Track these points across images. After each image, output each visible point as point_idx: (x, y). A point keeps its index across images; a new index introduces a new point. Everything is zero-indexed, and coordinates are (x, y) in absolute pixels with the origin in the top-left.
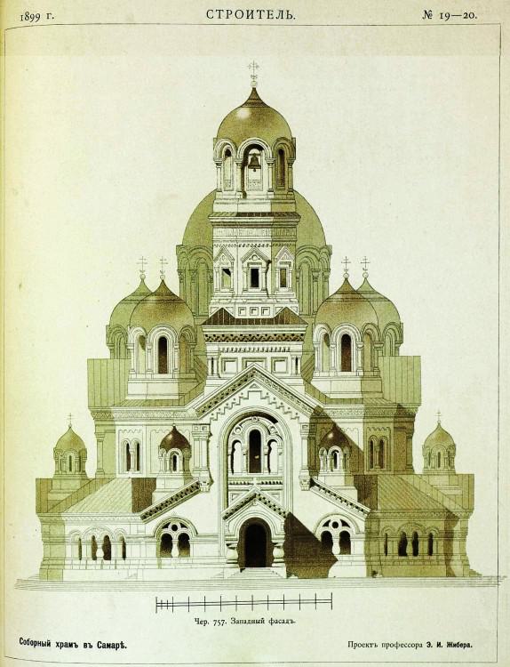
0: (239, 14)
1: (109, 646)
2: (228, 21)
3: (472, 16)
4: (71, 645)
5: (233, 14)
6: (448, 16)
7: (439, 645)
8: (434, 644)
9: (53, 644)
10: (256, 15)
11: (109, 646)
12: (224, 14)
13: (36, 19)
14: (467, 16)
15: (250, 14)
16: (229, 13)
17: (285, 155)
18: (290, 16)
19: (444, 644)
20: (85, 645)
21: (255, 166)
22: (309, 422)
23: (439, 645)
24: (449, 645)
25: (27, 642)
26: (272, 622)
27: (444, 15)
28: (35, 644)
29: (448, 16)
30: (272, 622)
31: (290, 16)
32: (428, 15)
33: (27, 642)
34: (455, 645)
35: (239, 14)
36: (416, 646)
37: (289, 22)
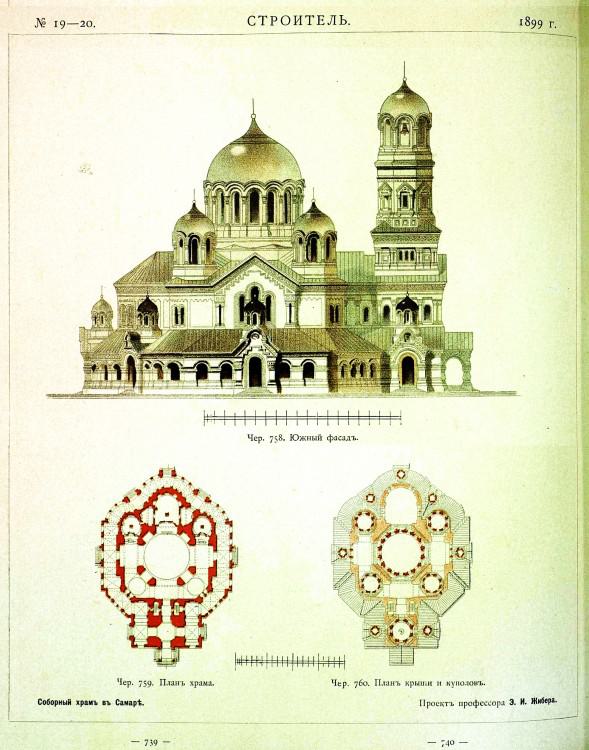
0: (286, 21)
1: (126, 703)
2: (62, 32)
3: (89, 24)
4: (91, 703)
5: (279, 19)
6: (63, 24)
7: (522, 701)
8: (517, 701)
9: (74, 702)
10: (305, 21)
11: (126, 703)
12: (267, 21)
13: (537, 26)
14: (84, 24)
15: (298, 21)
16: (273, 19)
17: (425, 122)
18: (344, 22)
19: (528, 701)
20: (104, 703)
21: (406, 130)
22: (278, 327)
23: (522, 701)
24: (534, 701)
25: (47, 702)
26: (330, 438)
27: (58, 23)
28: (55, 703)
29: (63, 24)
30: (330, 438)
31: (344, 22)
32: (41, 23)
33: (47, 702)
34: (540, 702)
35: (286, 21)
36: (497, 704)
37: (344, 28)
